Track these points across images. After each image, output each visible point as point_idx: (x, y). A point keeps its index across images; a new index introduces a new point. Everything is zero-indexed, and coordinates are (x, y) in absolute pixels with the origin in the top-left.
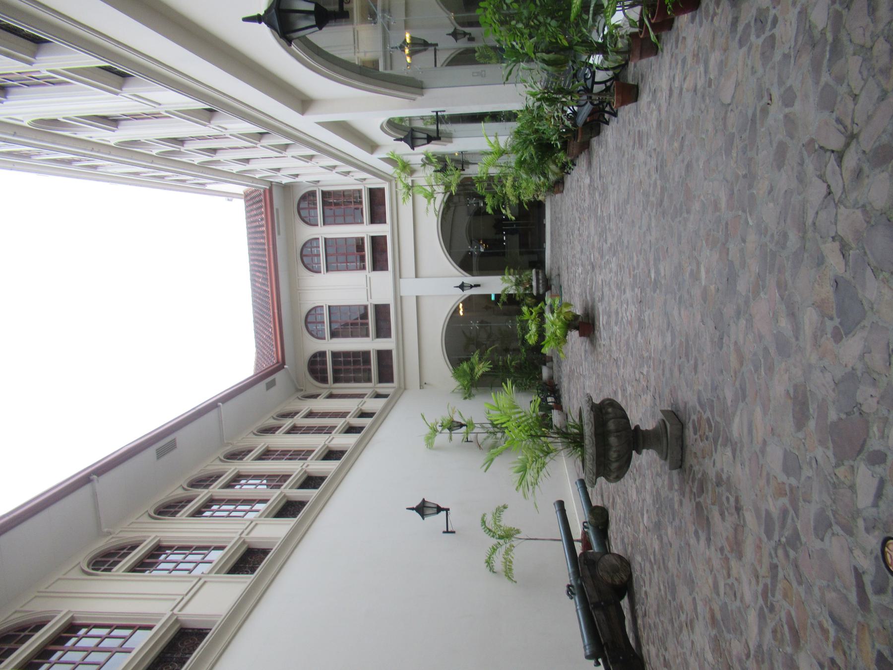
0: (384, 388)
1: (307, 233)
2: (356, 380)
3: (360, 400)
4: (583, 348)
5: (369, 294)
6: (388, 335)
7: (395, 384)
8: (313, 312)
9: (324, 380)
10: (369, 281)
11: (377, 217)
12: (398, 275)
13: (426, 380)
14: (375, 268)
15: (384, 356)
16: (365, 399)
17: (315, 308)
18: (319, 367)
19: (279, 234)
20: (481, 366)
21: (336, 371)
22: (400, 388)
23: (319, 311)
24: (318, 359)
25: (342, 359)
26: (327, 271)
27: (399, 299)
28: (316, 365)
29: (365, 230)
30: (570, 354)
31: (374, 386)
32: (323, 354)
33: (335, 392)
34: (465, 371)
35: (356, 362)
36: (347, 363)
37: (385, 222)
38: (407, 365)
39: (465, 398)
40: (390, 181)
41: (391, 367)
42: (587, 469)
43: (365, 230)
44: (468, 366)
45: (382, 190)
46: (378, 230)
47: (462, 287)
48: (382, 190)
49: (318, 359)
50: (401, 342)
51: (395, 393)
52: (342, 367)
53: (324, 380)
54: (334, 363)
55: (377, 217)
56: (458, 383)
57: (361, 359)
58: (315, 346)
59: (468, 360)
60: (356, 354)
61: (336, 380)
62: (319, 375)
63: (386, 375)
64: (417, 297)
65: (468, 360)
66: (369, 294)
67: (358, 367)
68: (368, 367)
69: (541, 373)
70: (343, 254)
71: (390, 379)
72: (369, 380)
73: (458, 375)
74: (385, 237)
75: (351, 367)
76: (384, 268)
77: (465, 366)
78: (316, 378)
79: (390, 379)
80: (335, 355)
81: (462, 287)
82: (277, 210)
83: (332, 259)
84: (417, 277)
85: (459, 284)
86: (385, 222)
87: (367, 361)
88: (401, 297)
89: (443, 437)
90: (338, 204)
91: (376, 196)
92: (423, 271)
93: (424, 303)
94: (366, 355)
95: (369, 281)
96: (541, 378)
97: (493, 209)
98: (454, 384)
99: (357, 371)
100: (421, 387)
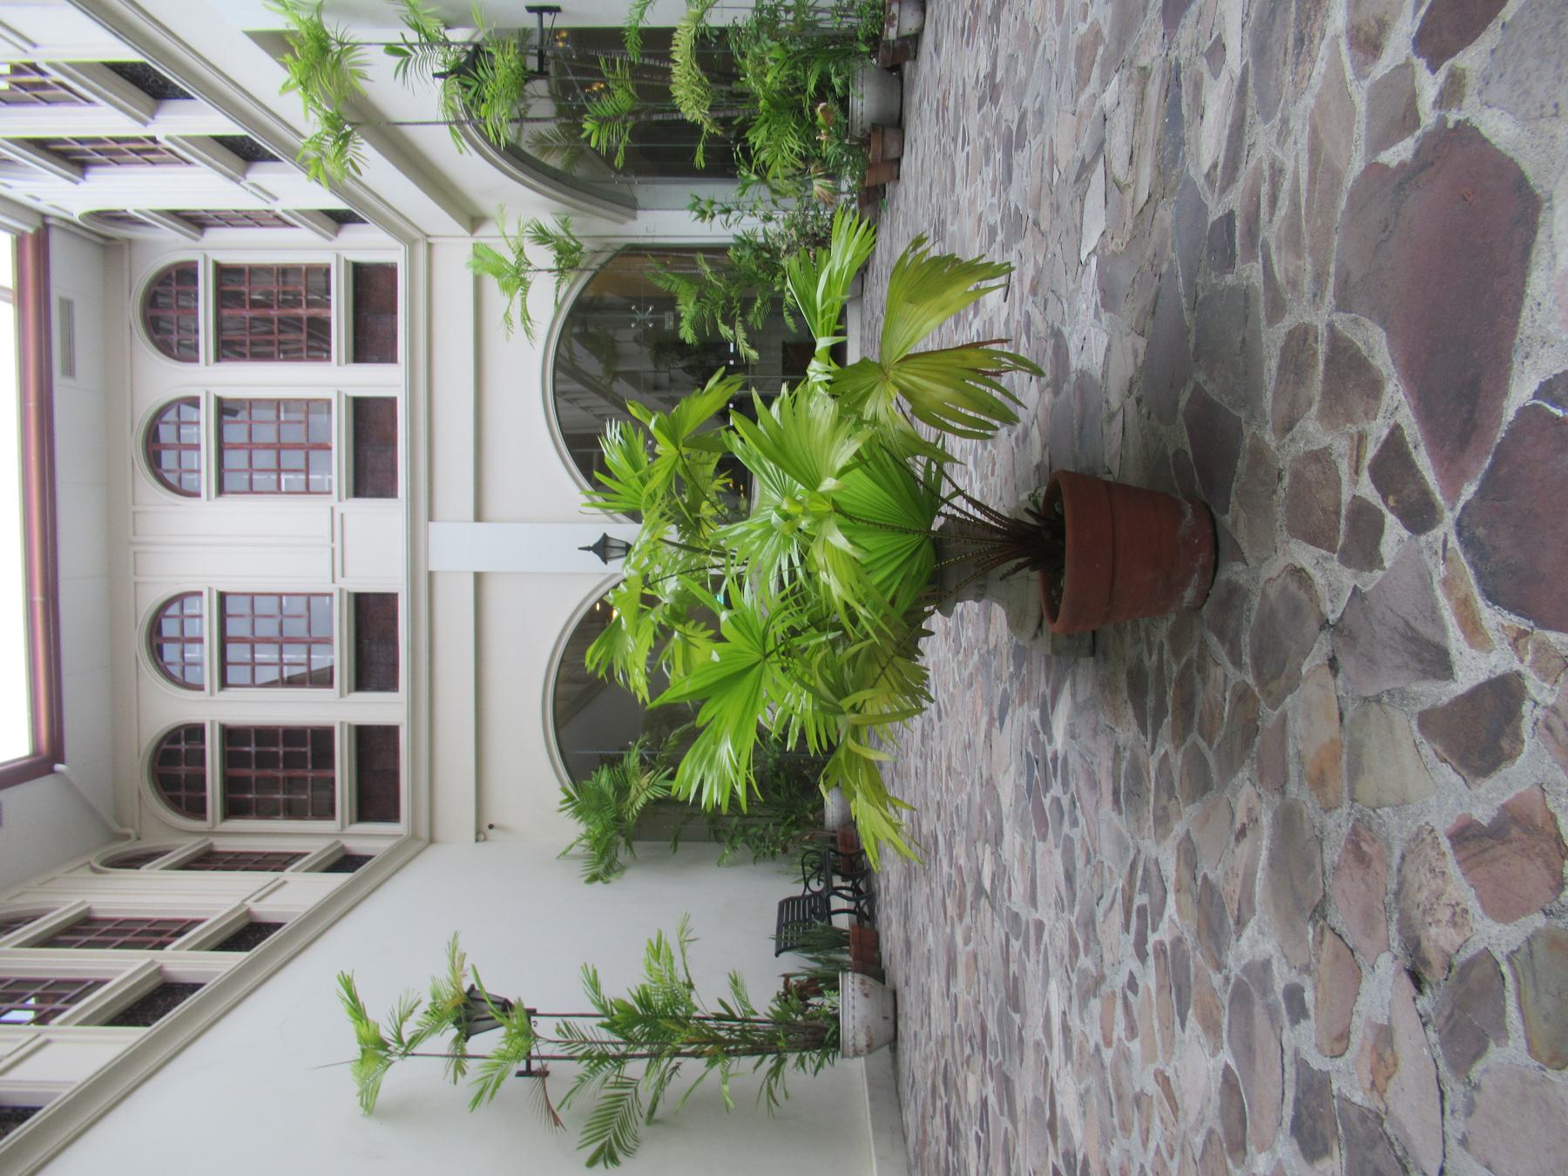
0: (370, 838)
1: (165, 379)
2: (293, 811)
3: (267, 877)
4: (1009, 739)
5: (339, 562)
6: (387, 355)
7: (400, 828)
8: (174, 610)
9: (196, 809)
10: (338, 527)
11: (372, 342)
12: (424, 512)
13: (492, 816)
14: (360, 487)
15: (375, 746)
16: (287, 874)
17: (180, 598)
18: (183, 770)
19: (69, 371)
20: (645, 781)
21: (231, 784)
22: (414, 836)
23: (191, 607)
24: (183, 746)
25: (252, 749)
26: (221, 490)
27: (424, 581)
28: (174, 764)
29: (340, 709)
30: (914, 762)
31: (341, 830)
32: (195, 732)
33: (223, 845)
34: (601, 794)
35: (292, 761)
36: (264, 760)
37: (394, 360)
38: (441, 771)
39: (594, 878)
40: (411, 243)
41: (396, 774)
42: (872, 841)
43: (335, 379)
44: (612, 780)
45: (389, 271)
46: (374, 380)
47: (603, 548)
48: (389, 271)
49: (183, 746)
50: (426, 706)
51: (391, 854)
52: (252, 772)
53: (196, 809)
54: (231, 759)
55: (372, 342)
56: (582, 828)
57: (308, 749)
58: (173, 706)
59: (614, 761)
60: (293, 735)
61: (234, 809)
62: (183, 793)
63: (377, 799)
64: (478, 577)
65: (614, 761)
66: (339, 562)
67: (299, 773)
68: (326, 773)
69: (821, 804)
70: (268, 447)
71: (389, 813)
72: (327, 812)
73: (582, 801)
74: (392, 402)
75: (274, 771)
76: (386, 489)
77: (604, 778)
78: (175, 804)
79: (389, 813)
80: (231, 735)
81: (603, 548)
82: (67, 305)
83: (235, 459)
84: (478, 517)
85: (594, 539)
86: (394, 360)
87: (324, 755)
88: (431, 575)
89: (420, 1073)
90: (270, 313)
91: (373, 288)
92: (492, 505)
93: (492, 590)
94: (323, 736)
95: (338, 527)
96: (821, 821)
97: (698, 328)
98: (573, 830)
99: (292, 784)
100: (480, 835)
